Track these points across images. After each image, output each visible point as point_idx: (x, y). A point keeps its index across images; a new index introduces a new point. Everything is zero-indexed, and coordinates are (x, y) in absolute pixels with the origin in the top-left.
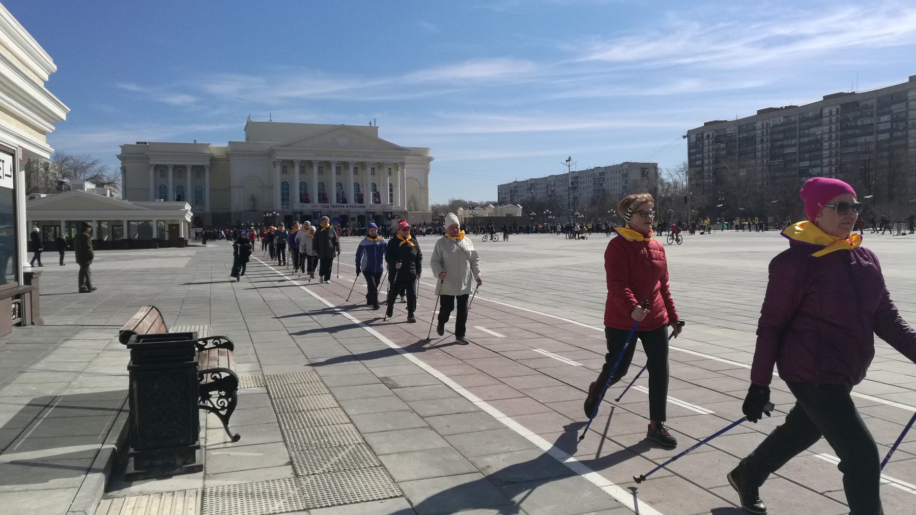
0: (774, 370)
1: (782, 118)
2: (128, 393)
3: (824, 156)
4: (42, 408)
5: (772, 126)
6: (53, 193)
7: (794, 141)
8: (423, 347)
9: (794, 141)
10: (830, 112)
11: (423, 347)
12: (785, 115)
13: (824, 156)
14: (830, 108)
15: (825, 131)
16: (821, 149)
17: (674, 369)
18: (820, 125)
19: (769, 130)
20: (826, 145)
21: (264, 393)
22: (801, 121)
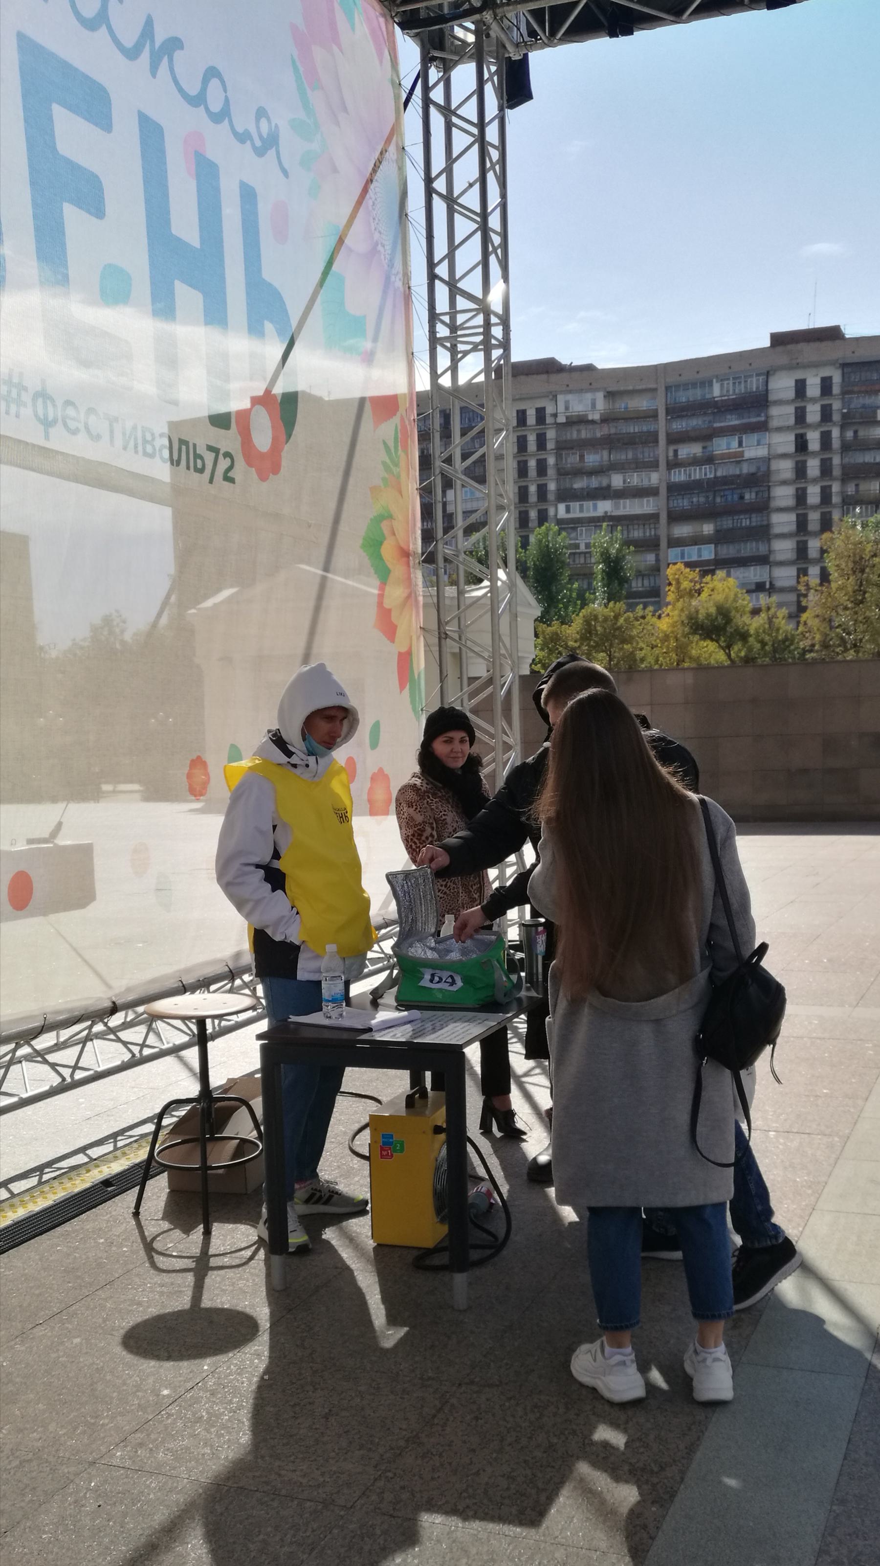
0: (290, 1228)
1: (600, 396)
2: (481, 912)
3: (776, 530)
4: (380, 951)
5: (561, 419)
6: (664, 1517)
7: (655, 478)
8: (493, 1119)
9: (655, 478)
10: (502, 506)
11: (493, 1119)
12: (610, 389)
13: (776, 530)
14: (799, 375)
15: (781, 450)
16: (763, 507)
17: (752, 1128)
18: (762, 427)
19: (551, 434)
20: (783, 495)
21: (814, 322)
22: (675, 411)
